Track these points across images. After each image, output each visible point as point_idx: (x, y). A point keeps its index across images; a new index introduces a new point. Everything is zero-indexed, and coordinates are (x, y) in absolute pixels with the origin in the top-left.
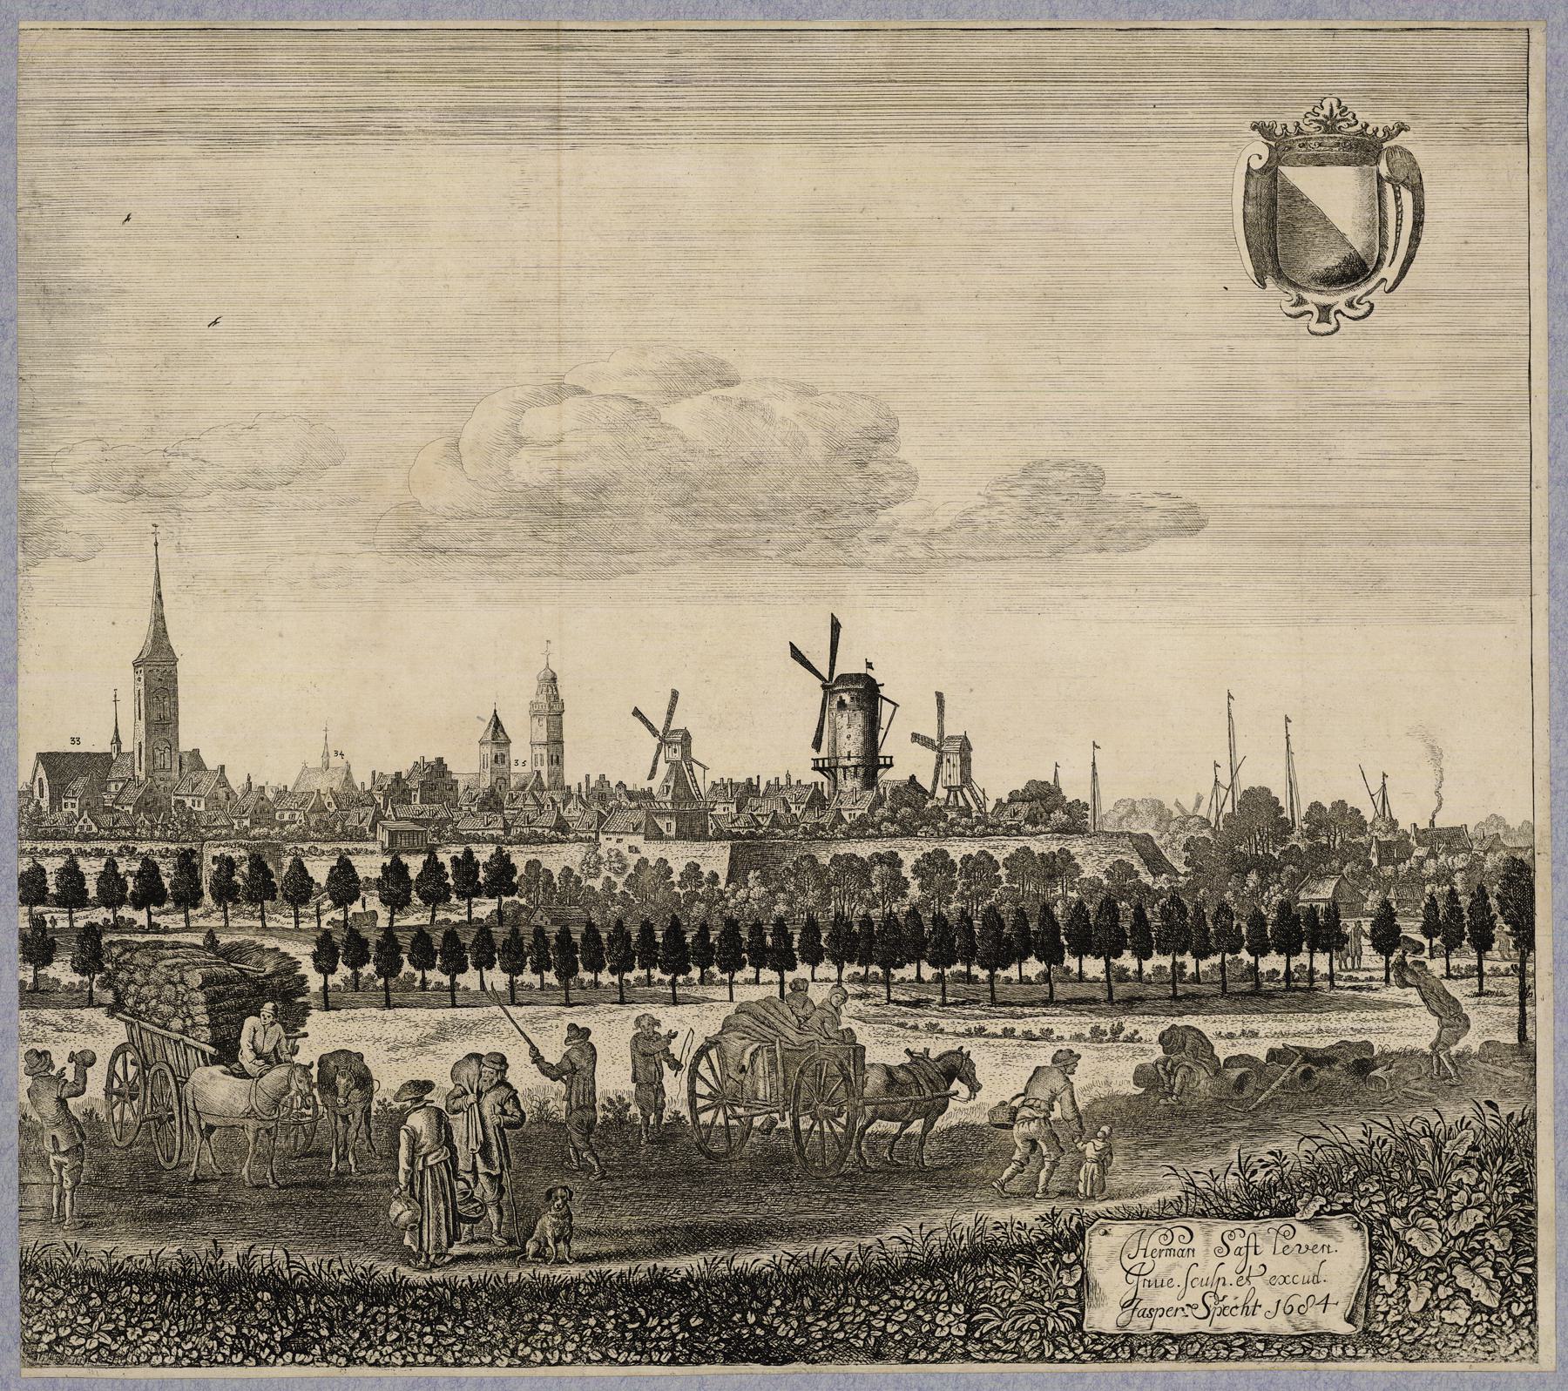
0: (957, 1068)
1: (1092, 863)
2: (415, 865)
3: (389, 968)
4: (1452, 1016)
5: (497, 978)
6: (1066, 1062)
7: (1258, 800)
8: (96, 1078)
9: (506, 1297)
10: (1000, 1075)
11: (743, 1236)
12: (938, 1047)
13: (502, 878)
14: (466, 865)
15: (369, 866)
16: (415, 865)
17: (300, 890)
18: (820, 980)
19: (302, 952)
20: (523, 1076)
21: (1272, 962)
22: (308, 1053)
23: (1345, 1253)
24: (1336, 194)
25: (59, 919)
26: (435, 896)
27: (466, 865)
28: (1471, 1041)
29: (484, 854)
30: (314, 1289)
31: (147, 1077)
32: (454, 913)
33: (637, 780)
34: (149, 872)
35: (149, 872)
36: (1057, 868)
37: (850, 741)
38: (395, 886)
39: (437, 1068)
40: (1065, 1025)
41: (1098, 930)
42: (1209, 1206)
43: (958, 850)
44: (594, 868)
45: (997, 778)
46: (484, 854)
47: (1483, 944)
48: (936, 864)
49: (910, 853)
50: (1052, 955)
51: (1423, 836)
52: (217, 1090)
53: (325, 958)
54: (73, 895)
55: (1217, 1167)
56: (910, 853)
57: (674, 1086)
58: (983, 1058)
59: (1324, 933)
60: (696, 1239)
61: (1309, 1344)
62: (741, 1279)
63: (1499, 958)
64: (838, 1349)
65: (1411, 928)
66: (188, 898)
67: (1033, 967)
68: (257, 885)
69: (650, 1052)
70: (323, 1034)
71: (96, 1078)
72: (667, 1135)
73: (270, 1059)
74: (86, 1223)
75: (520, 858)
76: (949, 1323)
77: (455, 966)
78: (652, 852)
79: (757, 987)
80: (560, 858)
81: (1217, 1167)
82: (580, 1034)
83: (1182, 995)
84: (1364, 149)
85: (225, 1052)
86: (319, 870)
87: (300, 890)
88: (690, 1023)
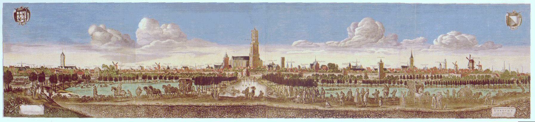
0: (480, 94)
1: (492, 76)
2: (433, 76)
3: (431, 84)
4: (523, 89)
5: (440, 85)
6: (490, 93)
7: (506, 70)
8: (406, 94)
9: (441, 113)
10: (484, 94)
11: (461, 108)
12: (479, 92)
13: (441, 77)
14: (438, 76)
15: (429, 76)
16: (433, 76)
17: (424, 78)
18: (468, 86)
19: (424, 83)
20: (443, 94)
21: (507, 85)
22: (424, 92)
23: (514, 110)
24: (514, 18)
25: (403, 80)
26: (435, 78)
27: (438, 76)
28: (525, 92)
29: (439, 75)
30: (425, 112)
31: (411, 94)
32: (437, 80)
33: (453, 68)
34: (411, 76)
35: (411, 76)
36: (489, 76)
37: (471, 65)
38: (432, 78)
39: (435, 93)
40: (490, 90)
41: (493, 82)
42: (502, 106)
43: (481, 75)
44: (449, 76)
45: (484, 69)
46: (439, 75)
47: (526, 83)
48: (479, 76)
49: (476, 75)
50: (489, 84)
51: (522, 74)
52: (417, 95)
53: (426, 84)
54: (404, 78)
55: (502, 102)
56: (476, 75)
57: (456, 95)
58: (483, 93)
59: (512, 82)
60: (458, 108)
61: (511, 118)
62: (461, 112)
63: (527, 85)
64: (469, 117)
65: (520, 82)
66: (414, 78)
67: (487, 85)
68: (419, 77)
69: (454, 92)
70: (425, 90)
71: (406, 94)
72: (455, 99)
73: (421, 92)
74: (405, 107)
75: (443, 75)
76: (480, 116)
77: (437, 84)
78: (454, 75)
79: (463, 86)
80: (446, 75)
81: (502, 102)
82: (448, 90)
83: (500, 87)
84: (516, 15)
85: (417, 91)
86: (425, 76)
87: (424, 78)
88: (457, 90)
